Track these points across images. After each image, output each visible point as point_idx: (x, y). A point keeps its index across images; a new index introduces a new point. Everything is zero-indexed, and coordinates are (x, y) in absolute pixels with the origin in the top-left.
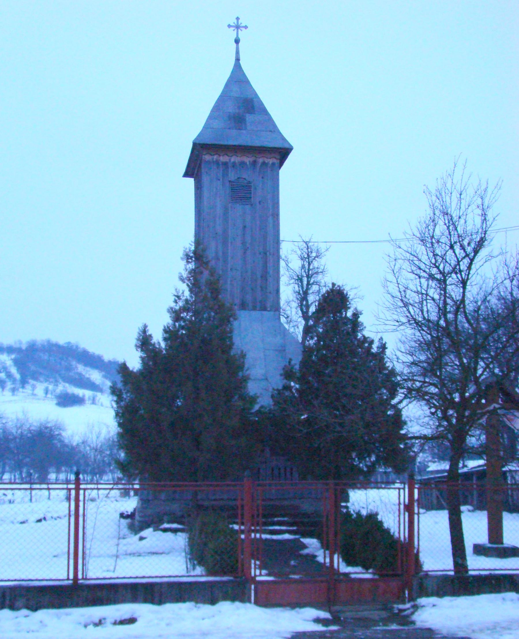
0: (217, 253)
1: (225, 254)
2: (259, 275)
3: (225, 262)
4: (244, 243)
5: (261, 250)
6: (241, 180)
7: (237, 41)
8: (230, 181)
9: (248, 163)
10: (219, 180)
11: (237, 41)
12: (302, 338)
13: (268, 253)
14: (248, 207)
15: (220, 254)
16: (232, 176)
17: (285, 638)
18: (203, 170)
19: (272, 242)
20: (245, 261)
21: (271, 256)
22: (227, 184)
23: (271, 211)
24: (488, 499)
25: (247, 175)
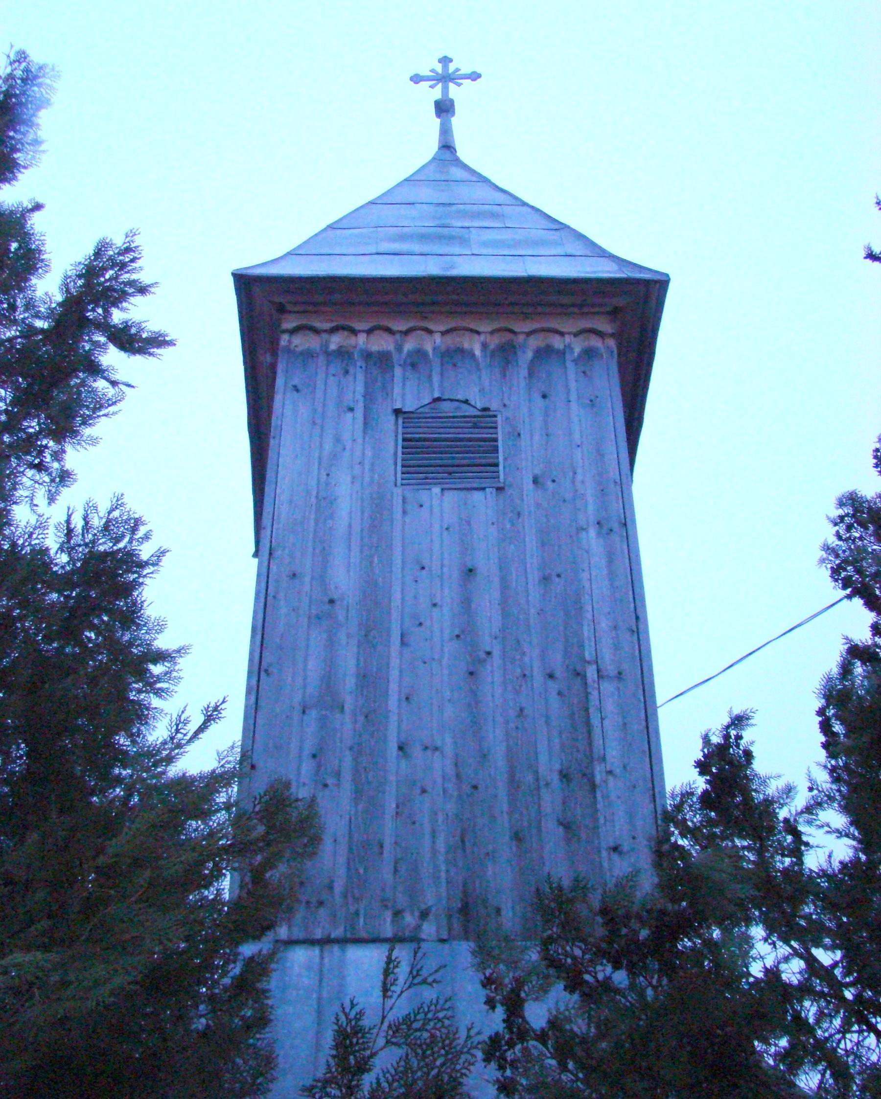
0: (329, 682)
1: (370, 681)
2: (548, 764)
3: (372, 718)
4: (465, 634)
5: (557, 659)
6: (446, 407)
7: (444, 108)
8: (397, 412)
9: (478, 352)
10: (351, 410)
11: (444, 108)
12: (815, 960)
13: (591, 673)
14: (482, 503)
15: (349, 683)
16: (409, 393)
17: (878, 1041)
18: (280, 381)
19: (604, 624)
20: (474, 701)
21: (607, 687)
22: (388, 424)
23: (591, 508)
24: (315, 996)
25: (475, 389)
